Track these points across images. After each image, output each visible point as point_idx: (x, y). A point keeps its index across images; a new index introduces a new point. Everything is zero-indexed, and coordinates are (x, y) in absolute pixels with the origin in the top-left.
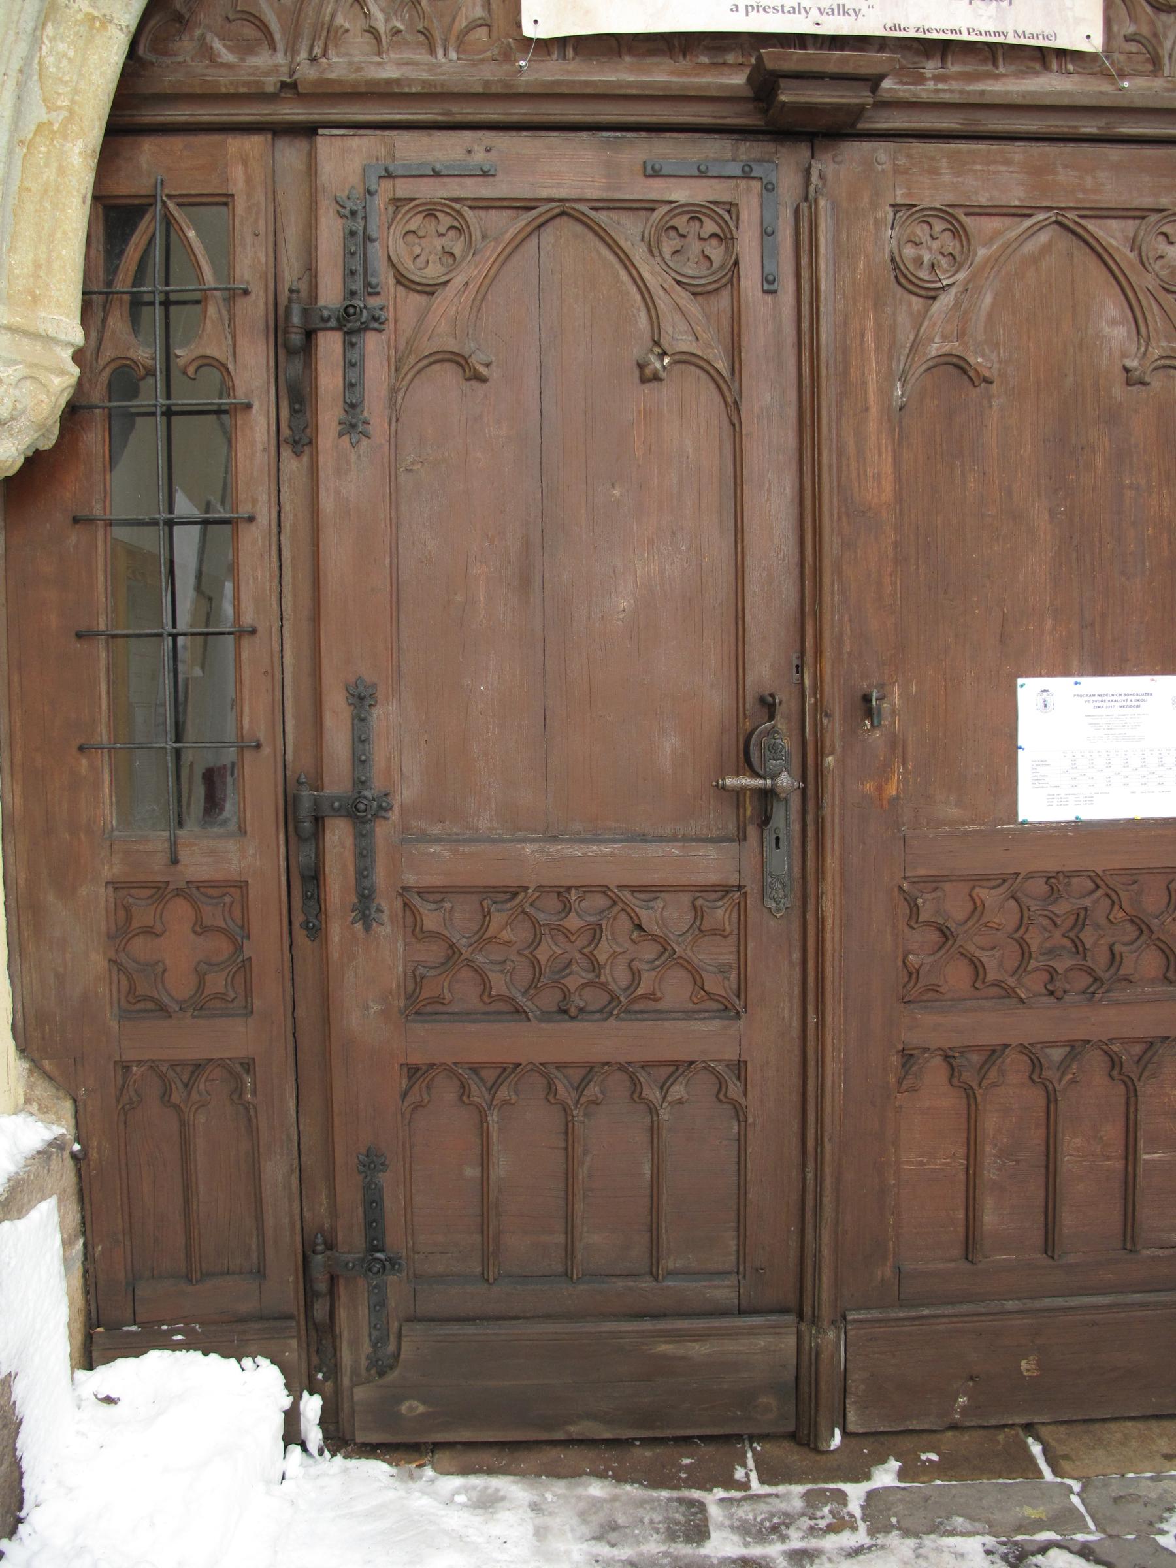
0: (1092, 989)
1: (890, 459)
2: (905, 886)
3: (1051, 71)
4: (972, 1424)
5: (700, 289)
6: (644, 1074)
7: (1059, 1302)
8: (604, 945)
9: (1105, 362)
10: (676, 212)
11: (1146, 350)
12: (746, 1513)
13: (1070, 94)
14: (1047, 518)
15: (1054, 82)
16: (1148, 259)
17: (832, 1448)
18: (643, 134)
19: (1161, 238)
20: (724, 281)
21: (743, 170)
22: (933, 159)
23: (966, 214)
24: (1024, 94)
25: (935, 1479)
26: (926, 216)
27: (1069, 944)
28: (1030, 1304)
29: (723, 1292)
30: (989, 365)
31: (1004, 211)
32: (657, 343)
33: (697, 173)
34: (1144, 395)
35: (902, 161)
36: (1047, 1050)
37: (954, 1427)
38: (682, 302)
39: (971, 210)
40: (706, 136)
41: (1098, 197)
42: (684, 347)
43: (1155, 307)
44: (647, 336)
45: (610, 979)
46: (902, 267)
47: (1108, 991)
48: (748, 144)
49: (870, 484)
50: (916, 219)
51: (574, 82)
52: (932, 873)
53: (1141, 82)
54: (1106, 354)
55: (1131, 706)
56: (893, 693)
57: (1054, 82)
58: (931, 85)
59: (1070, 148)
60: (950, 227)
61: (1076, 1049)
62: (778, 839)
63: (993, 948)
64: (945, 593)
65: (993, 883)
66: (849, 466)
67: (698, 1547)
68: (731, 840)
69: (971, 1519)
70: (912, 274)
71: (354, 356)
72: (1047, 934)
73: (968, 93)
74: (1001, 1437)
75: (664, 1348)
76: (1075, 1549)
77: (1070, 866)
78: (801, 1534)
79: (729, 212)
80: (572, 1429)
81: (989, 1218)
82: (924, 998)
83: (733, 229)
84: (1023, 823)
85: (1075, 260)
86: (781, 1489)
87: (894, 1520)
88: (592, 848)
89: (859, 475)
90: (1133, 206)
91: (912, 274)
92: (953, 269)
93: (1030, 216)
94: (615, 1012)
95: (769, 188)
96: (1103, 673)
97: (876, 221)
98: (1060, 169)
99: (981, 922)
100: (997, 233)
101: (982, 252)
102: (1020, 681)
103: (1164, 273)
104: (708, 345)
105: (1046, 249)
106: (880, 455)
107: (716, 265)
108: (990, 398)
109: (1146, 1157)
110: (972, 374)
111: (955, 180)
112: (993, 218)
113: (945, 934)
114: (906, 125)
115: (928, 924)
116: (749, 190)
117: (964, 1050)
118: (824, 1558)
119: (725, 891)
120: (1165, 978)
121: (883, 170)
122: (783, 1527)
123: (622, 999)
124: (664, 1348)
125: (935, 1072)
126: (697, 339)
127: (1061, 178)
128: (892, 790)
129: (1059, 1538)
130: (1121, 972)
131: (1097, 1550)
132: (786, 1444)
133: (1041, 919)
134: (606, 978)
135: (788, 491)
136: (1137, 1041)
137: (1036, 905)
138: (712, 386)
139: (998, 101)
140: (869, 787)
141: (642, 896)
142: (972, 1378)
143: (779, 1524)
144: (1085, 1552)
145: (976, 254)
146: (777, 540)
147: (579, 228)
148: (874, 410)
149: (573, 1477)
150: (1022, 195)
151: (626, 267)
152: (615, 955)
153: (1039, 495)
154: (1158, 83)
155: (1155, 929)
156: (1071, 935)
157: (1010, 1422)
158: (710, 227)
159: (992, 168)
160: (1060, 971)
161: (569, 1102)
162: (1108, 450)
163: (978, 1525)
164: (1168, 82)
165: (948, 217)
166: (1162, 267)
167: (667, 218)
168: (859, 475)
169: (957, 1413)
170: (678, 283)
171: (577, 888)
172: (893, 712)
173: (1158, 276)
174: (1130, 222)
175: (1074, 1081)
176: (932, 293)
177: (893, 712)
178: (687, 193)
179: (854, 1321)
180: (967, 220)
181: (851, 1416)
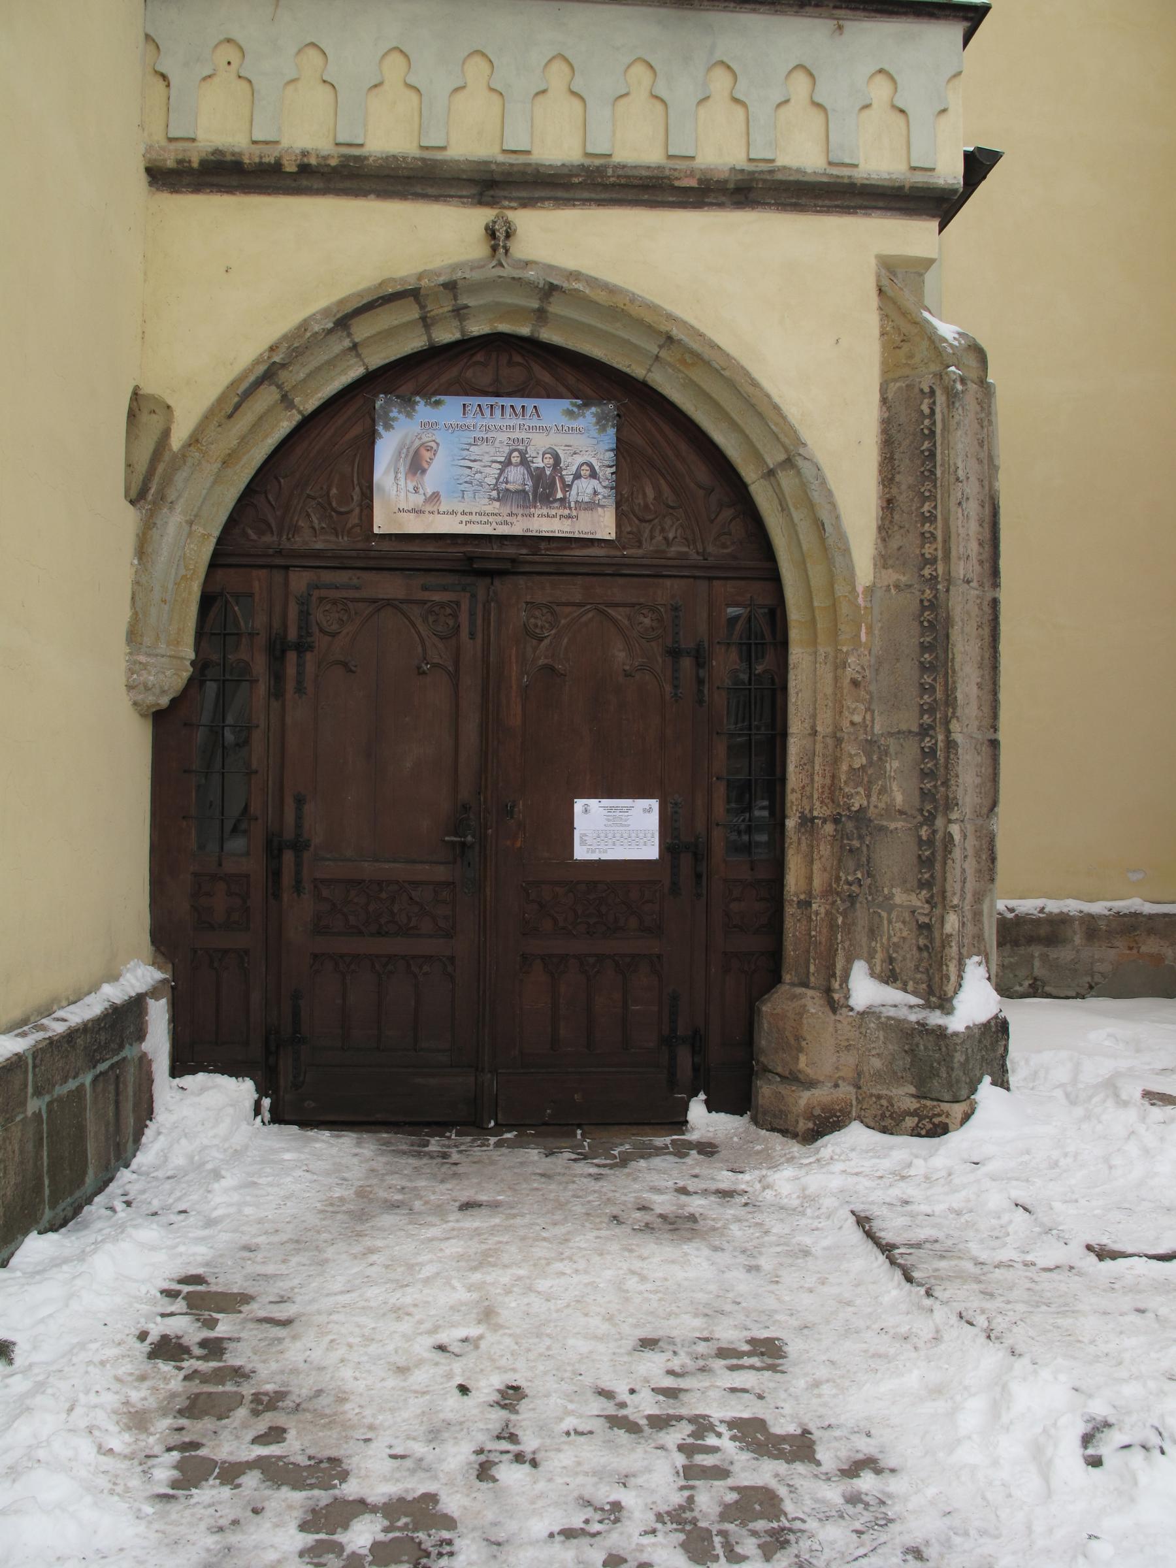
32: (425, 659)
42: (435, 661)
88: (392, 865)
95: (473, 596)
101: (563, 621)
128: (518, 844)
148: (514, 687)
158: (449, 611)
181: (500, 1116)
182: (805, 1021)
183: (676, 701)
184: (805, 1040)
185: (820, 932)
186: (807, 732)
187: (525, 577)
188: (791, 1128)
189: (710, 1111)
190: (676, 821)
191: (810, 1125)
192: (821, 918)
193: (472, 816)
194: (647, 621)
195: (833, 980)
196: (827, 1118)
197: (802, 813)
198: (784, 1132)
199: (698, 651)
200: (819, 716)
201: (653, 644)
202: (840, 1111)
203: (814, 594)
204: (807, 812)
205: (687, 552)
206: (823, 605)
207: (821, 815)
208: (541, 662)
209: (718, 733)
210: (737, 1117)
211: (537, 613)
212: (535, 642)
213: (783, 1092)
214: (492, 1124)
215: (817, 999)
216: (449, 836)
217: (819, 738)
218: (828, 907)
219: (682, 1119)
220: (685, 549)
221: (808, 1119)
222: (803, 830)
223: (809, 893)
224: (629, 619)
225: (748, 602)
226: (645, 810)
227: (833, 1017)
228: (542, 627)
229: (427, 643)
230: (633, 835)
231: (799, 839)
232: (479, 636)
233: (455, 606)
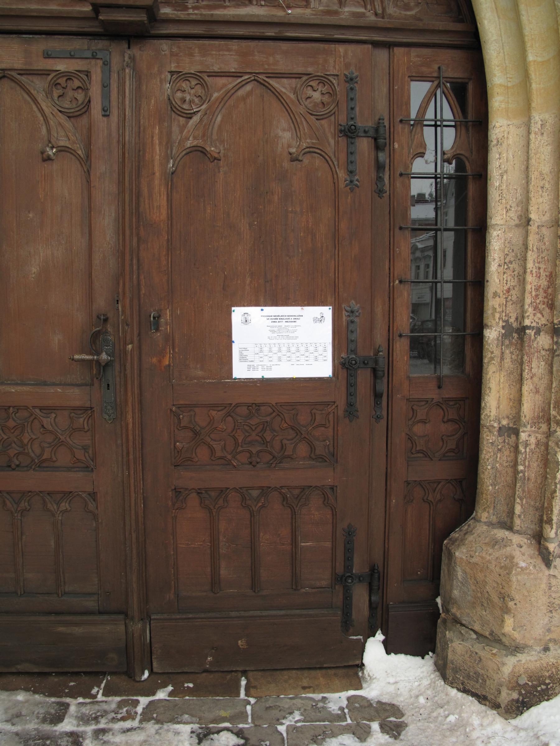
0: (271, 462)
1: (165, 198)
2: (174, 409)
3: (253, 5)
4: (216, 670)
5: (71, 115)
6: (48, 497)
7: (258, 613)
8: (26, 435)
9: (279, 149)
10: (59, 76)
11: (300, 143)
12: (86, 710)
13: (258, 16)
14: (248, 228)
15: (254, 10)
16: (301, 98)
17: (143, 679)
18: (44, 36)
19: (309, 88)
20: (83, 110)
21: (93, 55)
22: (191, 48)
23: (208, 76)
24: (234, 16)
25: (186, 696)
26: (187, 77)
27: (259, 439)
28: (242, 613)
29: (91, 603)
30: (218, 151)
31: (228, 74)
32: (50, 142)
33: (69, 56)
34: (299, 166)
35: (175, 50)
36: (250, 491)
37: (206, 671)
38: (62, 121)
39: (211, 74)
40: (75, 37)
41: (276, 68)
42: (62, 143)
43: (304, 123)
44: (46, 138)
45: (30, 451)
46: (174, 103)
47: (280, 463)
48: (96, 41)
49: (155, 211)
50: (182, 79)
51: (4, 9)
52: (187, 403)
53: (299, 11)
54: (280, 146)
55: (291, 322)
56: (166, 314)
57: (254, 10)
58: (191, 11)
59: (261, 43)
60: (199, 82)
61: (265, 491)
62: (108, 385)
63: (220, 440)
64: (195, 264)
65: (220, 408)
66: (144, 201)
67: (54, 726)
68: (86, 385)
69: (192, 715)
70: (179, 106)
71: (352, 158)
72: (247, 434)
73: (205, 15)
74: (228, 677)
75: (61, 629)
76: (235, 731)
77: (259, 400)
78: (106, 721)
79: (87, 76)
80: (19, 667)
81: (223, 572)
82: (186, 464)
83: (88, 84)
84: (235, 379)
85: (265, 98)
86: (110, 699)
87: (155, 715)
88: (19, 388)
89: (150, 207)
90: (294, 72)
91: (179, 106)
92: (200, 104)
93: (241, 77)
94: (33, 467)
95: (106, 64)
96: (276, 304)
97: (161, 81)
98: (256, 53)
99: (212, 427)
100: (225, 85)
101: (216, 95)
102: (233, 308)
103: (310, 106)
104: (74, 143)
105: (249, 94)
106: (160, 196)
107: (80, 102)
108: (219, 168)
109: (303, 544)
110: (209, 155)
111: (202, 59)
112: (223, 78)
113: (196, 434)
114: (176, 32)
115: (185, 428)
116: (96, 65)
117: (207, 490)
118: (111, 733)
119: (85, 409)
120: (310, 456)
121: (165, 54)
122: (100, 717)
123: (36, 461)
124: (61, 629)
125: (193, 500)
126: (69, 140)
127: (256, 58)
128: (166, 362)
129: (231, 726)
130: (286, 454)
131: (245, 732)
132: (123, 677)
133: (245, 427)
134: (28, 450)
135: (113, 215)
136: (296, 488)
137: (241, 420)
138: (78, 162)
139: (220, 19)
140: (154, 360)
141: (44, 411)
142: (213, 648)
143: (99, 716)
144: (239, 734)
145: (211, 96)
146: (108, 239)
147: (13, 84)
148: (157, 174)
149: (14, 690)
150: (236, 66)
151: (35, 104)
152: (32, 440)
153: (244, 216)
154: (308, 11)
155: (303, 433)
156: (260, 435)
157: (234, 670)
158: (77, 83)
159: (221, 53)
160: (254, 452)
161: (13, 509)
162: (280, 193)
163: (194, 719)
164: (313, 10)
165: (198, 78)
166: (310, 103)
167: (55, 79)
168: (150, 207)
169: (207, 664)
170: (60, 111)
171: (14, 407)
172: (166, 324)
173: (306, 107)
174: (294, 80)
175: (263, 507)
176: (189, 116)
177: (166, 324)
178: (65, 66)
179: (155, 619)
180: (206, 78)
181: (155, 664)
182: (514, 579)
183: (352, 190)
184: (512, 600)
185: (529, 466)
186: (513, 223)
187: (169, 42)
188: (490, 697)
189: (388, 653)
190: (352, 332)
191: (515, 696)
192: (531, 450)
193: (110, 329)
194: (317, 96)
195: (547, 527)
196: (535, 687)
197: (507, 321)
198: (482, 699)
199: (377, 130)
200: (533, 201)
201: (323, 122)
202: (550, 677)
203: (528, 45)
204: (512, 320)
205: (364, 14)
206: (539, 59)
207: (534, 324)
208: (189, 144)
209: (401, 228)
210: (419, 659)
211: (185, 85)
212: (182, 120)
213: (481, 653)
214: (146, 674)
215: (525, 547)
216: (82, 352)
217: (533, 228)
218: (539, 436)
219: (358, 662)
220: (362, 10)
221: (513, 689)
222: (507, 342)
223: (517, 417)
224: (295, 92)
225: (435, 75)
226: (316, 320)
227: (547, 572)
228: (191, 102)
229: (51, 123)
230: (302, 349)
231: (502, 353)
232: (115, 112)
233: (85, 77)
